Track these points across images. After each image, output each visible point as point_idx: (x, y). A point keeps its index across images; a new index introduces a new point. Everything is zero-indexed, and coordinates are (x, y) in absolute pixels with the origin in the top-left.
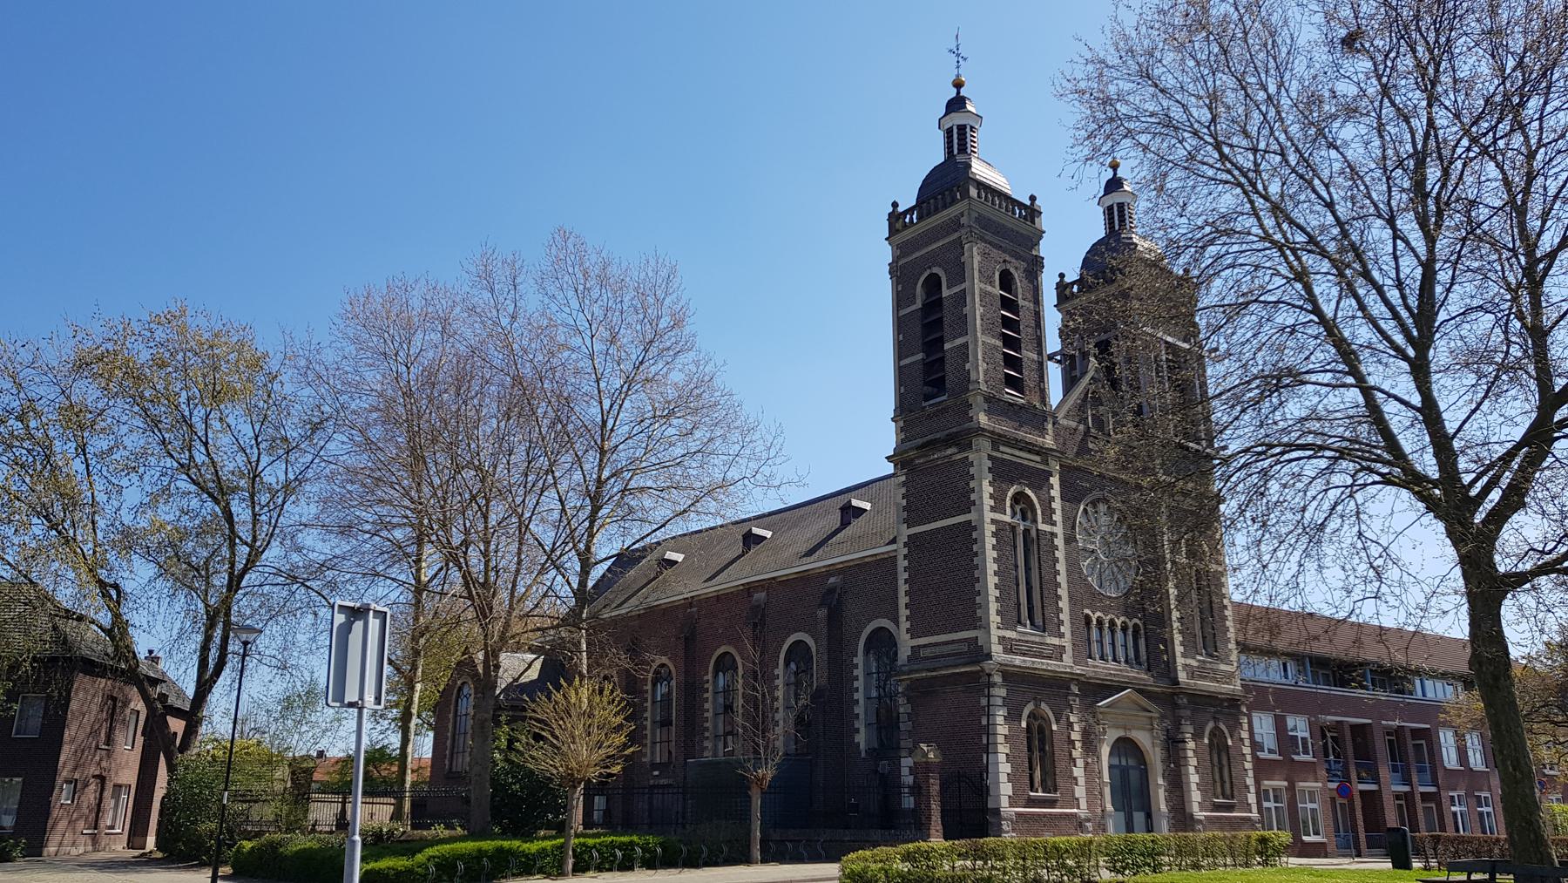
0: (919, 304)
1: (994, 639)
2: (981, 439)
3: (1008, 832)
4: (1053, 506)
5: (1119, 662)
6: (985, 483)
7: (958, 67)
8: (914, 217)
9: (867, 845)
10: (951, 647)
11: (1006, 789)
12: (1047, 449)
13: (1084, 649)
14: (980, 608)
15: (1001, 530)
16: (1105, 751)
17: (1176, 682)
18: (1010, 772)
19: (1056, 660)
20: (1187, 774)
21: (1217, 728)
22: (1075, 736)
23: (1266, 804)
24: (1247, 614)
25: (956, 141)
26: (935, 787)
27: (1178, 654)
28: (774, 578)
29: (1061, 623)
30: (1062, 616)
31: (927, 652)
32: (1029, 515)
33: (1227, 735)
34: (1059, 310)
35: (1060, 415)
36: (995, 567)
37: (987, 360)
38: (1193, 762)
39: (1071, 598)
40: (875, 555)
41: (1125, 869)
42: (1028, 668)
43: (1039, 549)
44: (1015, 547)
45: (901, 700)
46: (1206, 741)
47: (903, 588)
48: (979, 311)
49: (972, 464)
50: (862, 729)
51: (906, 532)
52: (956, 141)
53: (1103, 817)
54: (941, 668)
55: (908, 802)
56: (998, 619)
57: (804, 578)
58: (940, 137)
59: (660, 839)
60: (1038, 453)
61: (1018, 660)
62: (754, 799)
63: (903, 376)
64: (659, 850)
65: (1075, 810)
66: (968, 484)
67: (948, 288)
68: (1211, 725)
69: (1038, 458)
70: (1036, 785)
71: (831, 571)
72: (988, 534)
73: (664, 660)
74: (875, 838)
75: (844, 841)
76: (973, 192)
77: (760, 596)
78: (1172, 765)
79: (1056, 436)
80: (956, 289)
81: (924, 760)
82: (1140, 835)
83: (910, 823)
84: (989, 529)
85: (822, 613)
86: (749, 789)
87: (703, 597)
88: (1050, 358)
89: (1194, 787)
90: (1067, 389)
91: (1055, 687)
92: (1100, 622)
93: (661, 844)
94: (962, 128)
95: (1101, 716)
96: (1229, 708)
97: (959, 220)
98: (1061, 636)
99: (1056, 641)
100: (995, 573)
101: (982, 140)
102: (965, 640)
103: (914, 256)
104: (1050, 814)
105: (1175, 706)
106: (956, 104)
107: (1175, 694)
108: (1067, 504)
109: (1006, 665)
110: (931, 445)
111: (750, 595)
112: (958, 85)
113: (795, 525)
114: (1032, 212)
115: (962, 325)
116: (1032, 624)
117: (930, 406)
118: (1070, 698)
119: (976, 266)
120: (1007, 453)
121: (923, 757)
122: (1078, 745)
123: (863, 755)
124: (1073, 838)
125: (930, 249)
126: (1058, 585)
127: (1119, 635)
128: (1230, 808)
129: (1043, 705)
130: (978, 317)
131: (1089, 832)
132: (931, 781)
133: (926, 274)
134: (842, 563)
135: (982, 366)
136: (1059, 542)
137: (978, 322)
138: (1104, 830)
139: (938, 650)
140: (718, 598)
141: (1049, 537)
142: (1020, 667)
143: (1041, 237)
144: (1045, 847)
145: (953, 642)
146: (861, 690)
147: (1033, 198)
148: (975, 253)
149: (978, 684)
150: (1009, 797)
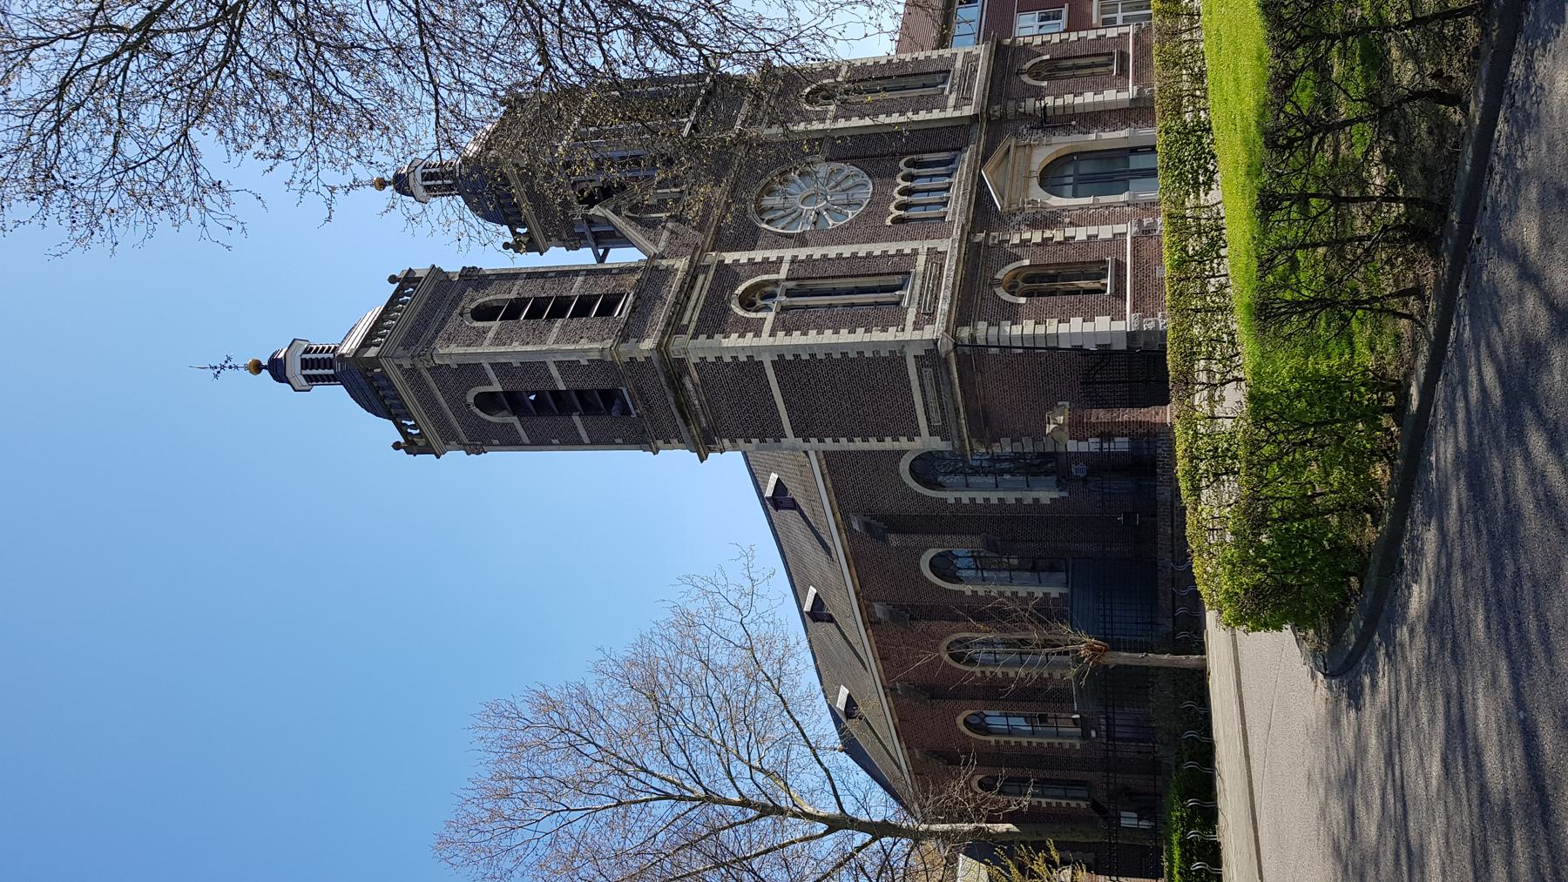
0: (514, 420)
1: (917, 335)
2: (671, 348)
3: (1157, 322)
4: (760, 260)
5: (950, 184)
6: (726, 343)
7: (236, 367)
8: (409, 423)
9: (1177, 504)
10: (928, 389)
11: (1103, 324)
12: (690, 267)
13: (934, 226)
14: (878, 352)
15: (785, 324)
16: (1055, 202)
17: (974, 119)
18: (1081, 319)
19: (944, 259)
20: (1084, 105)
21: (1029, 72)
22: (1037, 237)
23: (1119, 22)
24: (907, 37)
25: (320, 372)
26: (1100, 415)
27: (942, 115)
28: (857, 594)
29: (900, 253)
30: (892, 252)
31: (936, 417)
32: (768, 289)
33: (1038, 59)
34: (546, 251)
35: (653, 250)
36: (828, 332)
37: (577, 337)
38: (1069, 99)
39: (871, 240)
40: (823, 475)
41: (1207, 170)
42: (953, 294)
43: (809, 278)
44: (807, 307)
45: (996, 449)
46: (1045, 84)
47: (858, 445)
48: (517, 347)
49: (703, 359)
50: (1035, 494)
51: (790, 439)
52: (320, 372)
53: (1136, 205)
54: (955, 401)
55: (1121, 444)
56: (892, 330)
57: (855, 558)
58: (319, 390)
59: (1174, 796)
60: (695, 278)
61: (943, 306)
62: (1121, 662)
63: (602, 440)
64: (1191, 803)
65: (1129, 238)
66: (727, 365)
67: (490, 384)
68: (1025, 78)
69: (701, 278)
70: (1097, 285)
71: (845, 527)
72: (788, 341)
73: (960, 720)
74: (1168, 494)
75: (1172, 534)
76: (372, 352)
77: (879, 610)
78: (1073, 123)
79: (677, 255)
80: (491, 374)
81: (1066, 429)
82: (1159, 160)
83: (1148, 442)
84: (781, 339)
85: (894, 540)
86: (1106, 666)
87: (883, 677)
88: (601, 259)
89: (1099, 98)
90: (626, 242)
91: (977, 261)
92: (902, 206)
93: (1183, 798)
94: (306, 364)
95: (1014, 207)
96: (1006, 58)
97: (407, 370)
98: (915, 252)
99: (921, 259)
100: (805, 334)
101: (323, 337)
102: (919, 370)
103: (456, 424)
104: (1133, 269)
105: (1003, 119)
106: (277, 369)
107: (989, 120)
108: (759, 243)
109: (948, 321)
110: (683, 407)
111: (878, 622)
112: (257, 367)
113: (801, 560)
114: (407, 281)
115: (533, 368)
116: (900, 288)
117: (635, 409)
118: (991, 242)
119: (461, 350)
120: (691, 316)
121: (1062, 430)
122: (1048, 234)
123: (1065, 494)
124: (1165, 240)
125: (445, 405)
126: (854, 256)
127: (918, 184)
128: (1124, 57)
129: (999, 276)
130: (524, 348)
131: (1155, 222)
132: (1093, 420)
133: (477, 411)
134: (834, 515)
135: (584, 344)
136: (802, 253)
137: (529, 348)
138: (1153, 203)
139: (933, 404)
140: (883, 658)
141: (796, 266)
142: (951, 305)
143: (440, 270)
144: (1180, 280)
145: (922, 385)
146: (987, 495)
147: (393, 279)
148: (446, 351)
149: (971, 357)
150: (1112, 320)
